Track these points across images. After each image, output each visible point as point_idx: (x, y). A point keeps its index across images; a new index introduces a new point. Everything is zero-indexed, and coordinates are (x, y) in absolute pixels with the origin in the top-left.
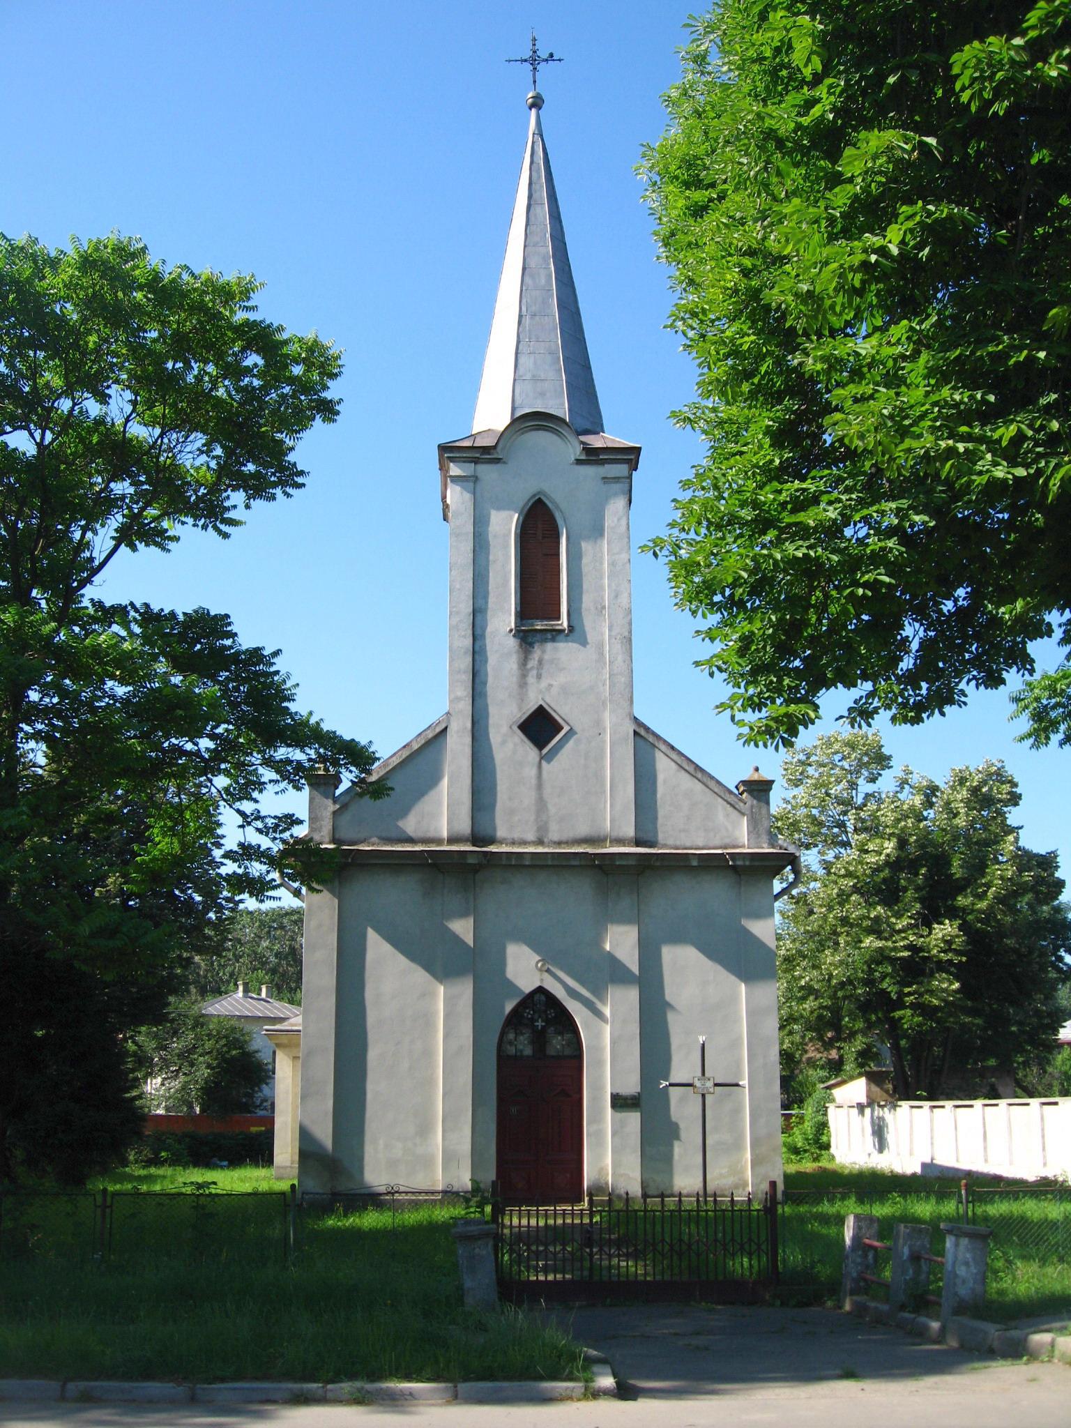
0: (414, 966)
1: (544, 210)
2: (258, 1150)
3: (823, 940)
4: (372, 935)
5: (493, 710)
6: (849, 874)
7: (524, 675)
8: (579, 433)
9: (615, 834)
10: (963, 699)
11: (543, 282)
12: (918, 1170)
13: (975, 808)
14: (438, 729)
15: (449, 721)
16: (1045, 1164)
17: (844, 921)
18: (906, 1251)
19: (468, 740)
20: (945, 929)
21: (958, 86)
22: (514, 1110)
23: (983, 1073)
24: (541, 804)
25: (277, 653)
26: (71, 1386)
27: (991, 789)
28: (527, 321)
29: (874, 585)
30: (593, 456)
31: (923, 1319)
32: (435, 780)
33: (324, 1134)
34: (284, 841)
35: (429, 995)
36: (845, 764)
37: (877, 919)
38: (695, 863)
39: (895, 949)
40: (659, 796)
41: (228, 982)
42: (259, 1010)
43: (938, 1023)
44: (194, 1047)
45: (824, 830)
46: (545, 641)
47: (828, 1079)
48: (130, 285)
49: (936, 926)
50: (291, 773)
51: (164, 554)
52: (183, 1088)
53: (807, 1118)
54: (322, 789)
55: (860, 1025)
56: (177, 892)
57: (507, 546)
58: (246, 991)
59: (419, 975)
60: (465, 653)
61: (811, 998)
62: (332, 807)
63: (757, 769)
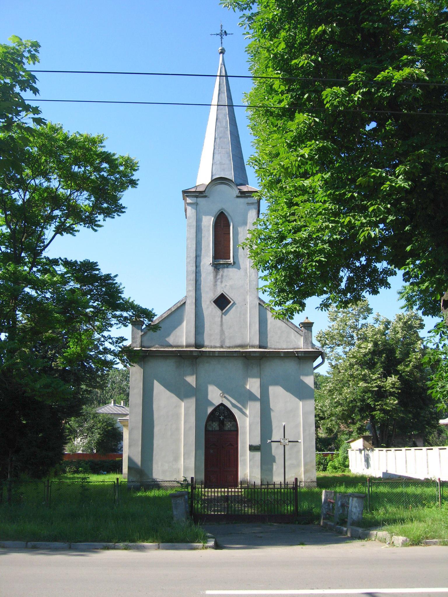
0: (173, 395)
1: (225, 95)
2: (117, 468)
3: (344, 383)
4: (155, 382)
5: (203, 295)
6: (354, 357)
7: (216, 282)
8: (237, 185)
9: (251, 344)
10: (364, 299)
11: (224, 124)
12: (381, 476)
13: (405, 330)
14: (182, 303)
15: (186, 299)
16: (428, 473)
17: (352, 376)
18: (339, 503)
19: (194, 307)
20: (392, 379)
21: (325, 102)
22: (212, 451)
23: (410, 437)
24: (222, 332)
25: (116, 276)
26: (29, 543)
27: (412, 322)
28: (218, 140)
29: (320, 262)
30: (243, 194)
31: (342, 528)
32: (180, 322)
33: (138, 460)
34: (120, 347)
35: (178, 406)
36: (354, 312)
37: (365, 375)
38: (282, 355)
39: (372, 387)
40: (268, 328)
41: (109, 399)
42: (120, 411)
43: (390, 416)
44: (93, 426)
45: (345, 339)
46: (224, 267)
47: (349, 439)
48: (56, 140)
49: (388, 378)
50: (124, 321)
51: (73, 237)
52: (89, 443)
53: (340, 454)
54: (137, 326)
55: (359, 417)
56: (85, 364)
57: (209, 231)
58: (114, 403)
59: (174, 398)
60: (193, 273)
61: (339, 406)
62: (140, 333)
63: (307, 318)
